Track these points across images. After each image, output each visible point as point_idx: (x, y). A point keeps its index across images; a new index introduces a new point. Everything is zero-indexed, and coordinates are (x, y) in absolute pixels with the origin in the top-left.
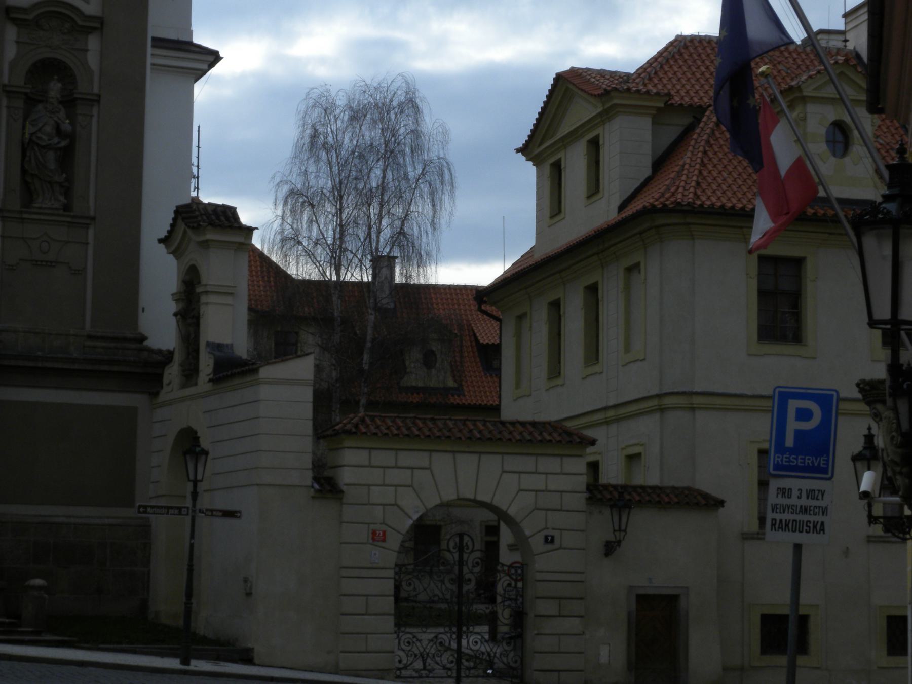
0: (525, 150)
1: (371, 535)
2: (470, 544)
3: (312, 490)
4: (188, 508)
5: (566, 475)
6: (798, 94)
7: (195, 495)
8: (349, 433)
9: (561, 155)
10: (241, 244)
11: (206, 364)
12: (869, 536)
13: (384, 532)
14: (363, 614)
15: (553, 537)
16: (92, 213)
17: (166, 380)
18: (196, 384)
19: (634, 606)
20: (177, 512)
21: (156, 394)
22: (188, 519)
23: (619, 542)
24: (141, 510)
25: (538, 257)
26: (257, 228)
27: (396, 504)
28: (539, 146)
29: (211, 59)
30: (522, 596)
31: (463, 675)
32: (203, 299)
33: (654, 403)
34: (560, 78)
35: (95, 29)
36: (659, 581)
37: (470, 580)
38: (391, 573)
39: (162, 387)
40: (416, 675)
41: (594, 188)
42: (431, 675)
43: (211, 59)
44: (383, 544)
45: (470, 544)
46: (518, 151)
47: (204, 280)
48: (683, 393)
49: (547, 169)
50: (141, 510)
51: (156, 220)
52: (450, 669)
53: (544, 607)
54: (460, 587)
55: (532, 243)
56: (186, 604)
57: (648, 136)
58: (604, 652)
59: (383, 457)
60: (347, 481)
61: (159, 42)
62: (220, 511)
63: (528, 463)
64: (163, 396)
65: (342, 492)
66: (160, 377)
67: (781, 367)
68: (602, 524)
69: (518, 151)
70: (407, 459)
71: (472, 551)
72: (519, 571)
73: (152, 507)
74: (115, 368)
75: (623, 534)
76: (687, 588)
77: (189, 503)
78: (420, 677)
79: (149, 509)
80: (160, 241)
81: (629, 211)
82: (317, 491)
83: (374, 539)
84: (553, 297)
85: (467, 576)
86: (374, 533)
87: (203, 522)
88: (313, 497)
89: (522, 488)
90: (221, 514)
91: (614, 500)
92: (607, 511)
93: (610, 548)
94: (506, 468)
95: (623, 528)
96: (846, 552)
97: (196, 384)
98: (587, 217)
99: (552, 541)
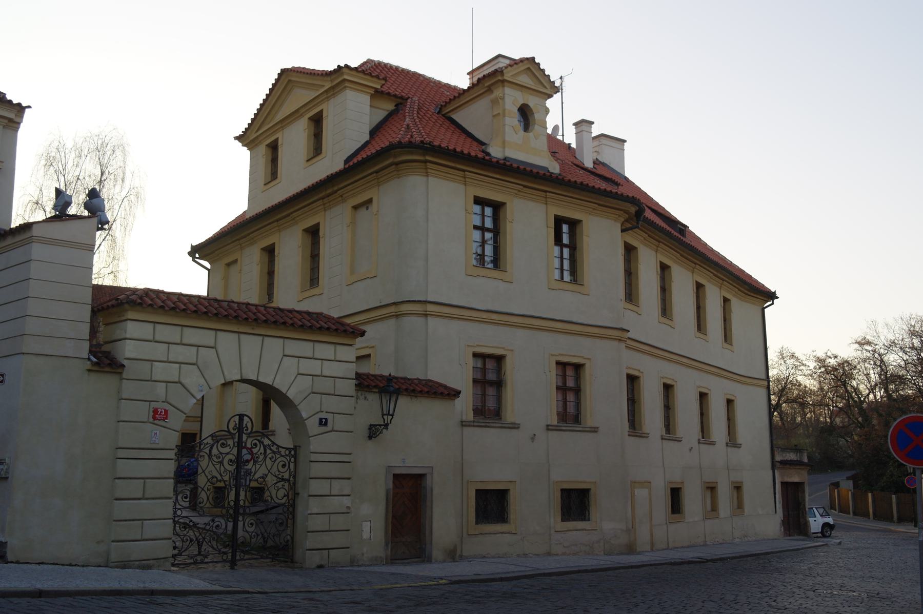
1: (152, 414)
2: (249, 425)
3: (89, 363)
5: (336, 361)
6: (500, 78)
9: (278, 135)
10: (11, 120)
12: (548, 426)
13: (166, 411)
14: (139, 499)
15: (326, 420)
19: (391, 485)
23: (386, 426)
25: (247, 217)
26: (29, 107)
30: (294, 477)
31: (238, 557)
33: (392, 309)
34: (284, 72)
36: (411, 463)
38: (172, 454)
40: (192, 561)
41: (317, 149)
42: (206, 560)
44: (162, 423)
45: (249, 425)
46: (236, 138)
49: (262, 149)
52: (225, 553)
53: (316, 487)
55: (246, 208)
57: (367, 109)
58: (366, 527)
63: (305, 348)
65: (123, 366)
67: (486, 291)
68: (370, 408)
69: (236, 138)
70: (192, 335)
72: (293, 453)
75: (390, 417)
78: (195, 563)
81: (383, 142)
82: (94, 364)
83: (154, 418)
84: (266, 243)
86: (155, 411)
88: (89, 370)
89: (301, 372)
92: (377, 396)
93: (373, 432)
94: (287, 353)
95: (391, 412)
99: (326, 424)
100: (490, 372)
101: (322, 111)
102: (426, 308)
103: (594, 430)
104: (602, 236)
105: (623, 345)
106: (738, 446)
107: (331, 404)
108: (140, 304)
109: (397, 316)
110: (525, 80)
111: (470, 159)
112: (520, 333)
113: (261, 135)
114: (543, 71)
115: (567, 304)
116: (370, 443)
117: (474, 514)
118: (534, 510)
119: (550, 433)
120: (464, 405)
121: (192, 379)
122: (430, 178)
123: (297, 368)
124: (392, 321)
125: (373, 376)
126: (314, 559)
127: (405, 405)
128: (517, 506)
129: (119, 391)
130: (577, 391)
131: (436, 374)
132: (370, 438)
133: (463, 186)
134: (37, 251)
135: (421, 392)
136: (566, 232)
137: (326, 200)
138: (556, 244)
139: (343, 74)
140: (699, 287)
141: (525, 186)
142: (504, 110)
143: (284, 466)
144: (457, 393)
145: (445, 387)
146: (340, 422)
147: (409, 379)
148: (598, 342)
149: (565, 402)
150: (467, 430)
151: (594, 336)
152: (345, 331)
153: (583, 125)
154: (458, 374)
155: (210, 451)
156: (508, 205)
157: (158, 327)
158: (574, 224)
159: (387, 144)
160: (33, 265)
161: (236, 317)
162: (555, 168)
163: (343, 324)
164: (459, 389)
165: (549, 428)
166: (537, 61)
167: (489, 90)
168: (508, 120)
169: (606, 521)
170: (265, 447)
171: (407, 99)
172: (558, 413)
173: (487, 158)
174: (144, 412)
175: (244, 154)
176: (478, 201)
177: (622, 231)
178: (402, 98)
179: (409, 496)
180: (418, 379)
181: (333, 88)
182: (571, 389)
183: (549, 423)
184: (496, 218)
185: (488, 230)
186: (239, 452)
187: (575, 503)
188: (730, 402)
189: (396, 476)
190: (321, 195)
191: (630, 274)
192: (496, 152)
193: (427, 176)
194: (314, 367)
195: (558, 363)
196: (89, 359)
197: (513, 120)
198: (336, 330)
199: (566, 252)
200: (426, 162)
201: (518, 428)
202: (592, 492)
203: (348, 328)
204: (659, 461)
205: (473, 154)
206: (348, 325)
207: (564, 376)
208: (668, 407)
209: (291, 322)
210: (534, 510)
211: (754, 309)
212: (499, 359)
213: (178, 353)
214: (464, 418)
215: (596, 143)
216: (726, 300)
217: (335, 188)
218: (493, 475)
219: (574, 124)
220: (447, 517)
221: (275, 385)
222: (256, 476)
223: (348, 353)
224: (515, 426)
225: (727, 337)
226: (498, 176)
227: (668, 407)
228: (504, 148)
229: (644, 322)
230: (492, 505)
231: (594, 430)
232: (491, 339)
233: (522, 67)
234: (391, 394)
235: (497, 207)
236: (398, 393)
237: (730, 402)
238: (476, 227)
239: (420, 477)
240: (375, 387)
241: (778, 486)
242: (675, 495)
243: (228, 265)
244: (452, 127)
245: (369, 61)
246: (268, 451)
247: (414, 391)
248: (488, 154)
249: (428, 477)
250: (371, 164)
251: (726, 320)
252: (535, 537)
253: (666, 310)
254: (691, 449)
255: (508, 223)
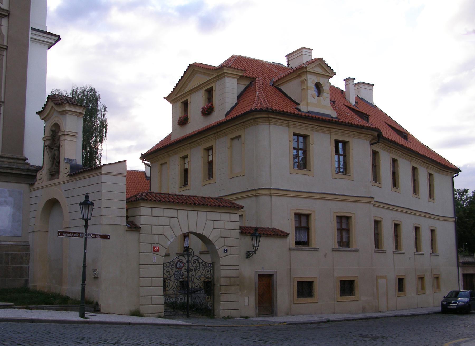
0: (168, 98)
4: (83, 233)
5: (230, 222)
7: (86, 226)
8: (143, 199)
11: (64, 169)
12: (333, 249)
13: (158, 247)
15: (227, 250)
16: (3, 100)
17: (38, 177)
18: (58, 178)
19: (257, 280)
20: (77, 235)
21: (32, 185)
22: (84, 239)
23: (255, 252)
24: (60, 234)
25: (173, 139)
27: (163, 234)
28: (176, 95)
29: (56, 38)
30: (213, 277)
32: (62, 138)
33: (254, 192)
34: (191, 66)
35: (6, 16)
36: (266, 270)
37: (192, 270)
38: (161, 267)
39: (36, 181)
43: (56, 38)
46: (165, 98)
47: (62, 129)
48: (268, 189)
49: (179, 104)
50: (60, 234)
51: (34, 103)
54: (188, 273)
56: (82, 285)
57: (236, 86)
59: (157, 212)
60: (142, 223)
61: (33, 29)
62: (100, 235)
64: (37, 185)
66: (35, 177)
67: (300, 181)
69: (165, 98)
71: (193, 256)
73: (65, 232)
74: (14, 172)
76: (276, 271)
77: (83, 231)
79: (63, 234)
80: (38, 113)
81: (229, 117)
82: (130, 227)
83: (154, 251)
85: (191, 268)
86: (154, 248)
87: (89, 240)
90: (100, 237)
91: (254, 233)
93: (249, 255)
94: (208, 219)
96: (325, 256)
97: (58, 178)
98: (197, 123)
99: (227, 251)
100: (303, 221)
101: (212, 87)
102: (271, 192)
103: (357, 250)
104: (360, 150)
105: (372, 205)
106: (437, 255)
107: (229, 242)
108: (146, 200)
109: (256, 196)
110: (318, 70)
111: (291, 115)
112: (318, 202)
113: (179, 97)
114: (327, 64)
115: (342, 186)
116: (247, 260)
117: (297, 293)
118: (326, 290)
119: (334, 252)
120: (291, 241)
121: (168, 233)
122: (271, 126)
123: (218, 227)
124: (254, 199)
125: (247, 227)
126: (223, 314)
127: (264, 242)
128: (317, 288)
129: (139, 238)
130: (348, 230)
131: (276, 225)
132: (247, 257)
133: (287, 128)
134: (104, 178)
135: (270, 235)
136: (341, 148)
137: (216, 135)
138: (336, 154)
139: (223, 70)
140: (414, 169)
141: (319, 126)
142: (307, 87)
143: (208, 271)
144: (288, 235)
145: (282, 232)
146: (233, 251)
147: (264, 228)
148: (359, 205)
149: (341, 237)
150: (293, 252)
151: (356, 202)
152: (235, 207)
153: (348, 80)
154: (287, 224)
155: (176, 265)
156: (311, 136)
157: (154, 209)
158: (345, 144)
159: (249, 109)
160: (103, 184)
161: (186, 203)
162: (334, 114)
163: (233, 204)
164: (288, 232)
165: (333, 250)
166: (324, 60)
167: (299, 76)
168: (310, 92)
169: (363, 295)
170: (199, 263)
171: (256, 79)
172: (338, 242)
173: (300, 113)
174: (149, 248)
175: (169, 107)
176: (295, 134)
177: (371, 144)
178: (253, 78)
179: (266, 284)
180: (268, 228)
181: (218, 76)
182: (344, 230)
183: (334, 247)
184: (305, 143)
185: (301, 149)
186: (189, 265)
187: (347, 287)
188: (432, 231)
189: (259, 276)
190: (214, 132)
191: (375, 166)
192: (303, 108)
193: (270, 124)
194: (219, 225)
195: (338, 217)
196: (126, 225)
197: (312, 91)
198: (230, 207)
199: (341, 158)
200: (269, 118)
201: (318, 250)
202: (356, 282)
203: (235, 205)
204: (391, 265)
205: (292, 112)
206: (235, 204)
207: (341, 223)
208: (397, 236)
209: (210, 204)
210: (326, 290)
211: (448, 179)
212: (308, 216)
213: (163, 221)
214: (291, 246)
215: (357, 87)
216: (430, 175)
217: (221, 129)
218: (305, 274)
219: (344, 80)
220: (284, 295)
221: (204, 234)
222: (196, 276)
223: (235, 217)
224: (316, 250)
225: (431, 195)
226: (306, 122)
227: (397, 236)
228: (308, 106)
229: (384, 192)
230: (305, 289)
231: (357, 250)
232: (304, 206)
233: (316, 63)
234: (257, 237)
235: (305, 137)
236: (260, 236)
237: (432, 231)
238: (294, 149)
239: (341, 281)
240: (249, 233)
241: (461, 276)
242: (401, 282)
243: (161, 165)
244: (280, 94)
245: (233, 57)
246: (201, 265)
247: (267, 234)
248: (300, 110)
249: (275, 276)
250: (241, 119)
251: (431, 186)
252: (326, 305)
253: (395, 184)
254: (325, 256)
255: (311, 145)
